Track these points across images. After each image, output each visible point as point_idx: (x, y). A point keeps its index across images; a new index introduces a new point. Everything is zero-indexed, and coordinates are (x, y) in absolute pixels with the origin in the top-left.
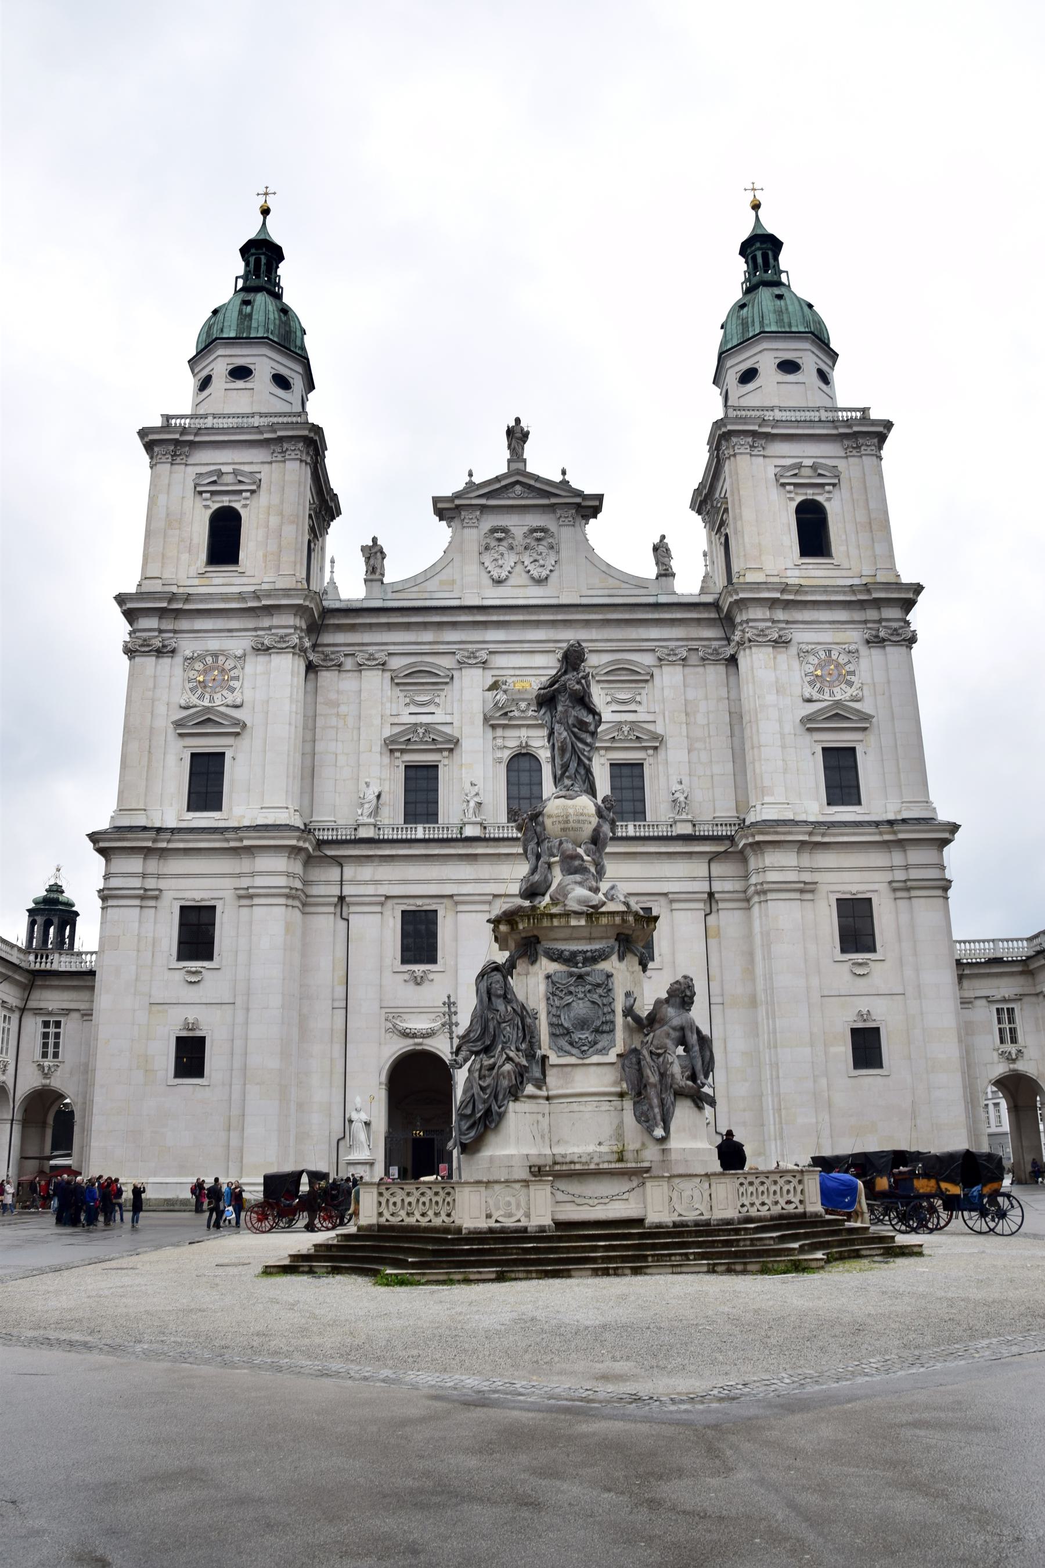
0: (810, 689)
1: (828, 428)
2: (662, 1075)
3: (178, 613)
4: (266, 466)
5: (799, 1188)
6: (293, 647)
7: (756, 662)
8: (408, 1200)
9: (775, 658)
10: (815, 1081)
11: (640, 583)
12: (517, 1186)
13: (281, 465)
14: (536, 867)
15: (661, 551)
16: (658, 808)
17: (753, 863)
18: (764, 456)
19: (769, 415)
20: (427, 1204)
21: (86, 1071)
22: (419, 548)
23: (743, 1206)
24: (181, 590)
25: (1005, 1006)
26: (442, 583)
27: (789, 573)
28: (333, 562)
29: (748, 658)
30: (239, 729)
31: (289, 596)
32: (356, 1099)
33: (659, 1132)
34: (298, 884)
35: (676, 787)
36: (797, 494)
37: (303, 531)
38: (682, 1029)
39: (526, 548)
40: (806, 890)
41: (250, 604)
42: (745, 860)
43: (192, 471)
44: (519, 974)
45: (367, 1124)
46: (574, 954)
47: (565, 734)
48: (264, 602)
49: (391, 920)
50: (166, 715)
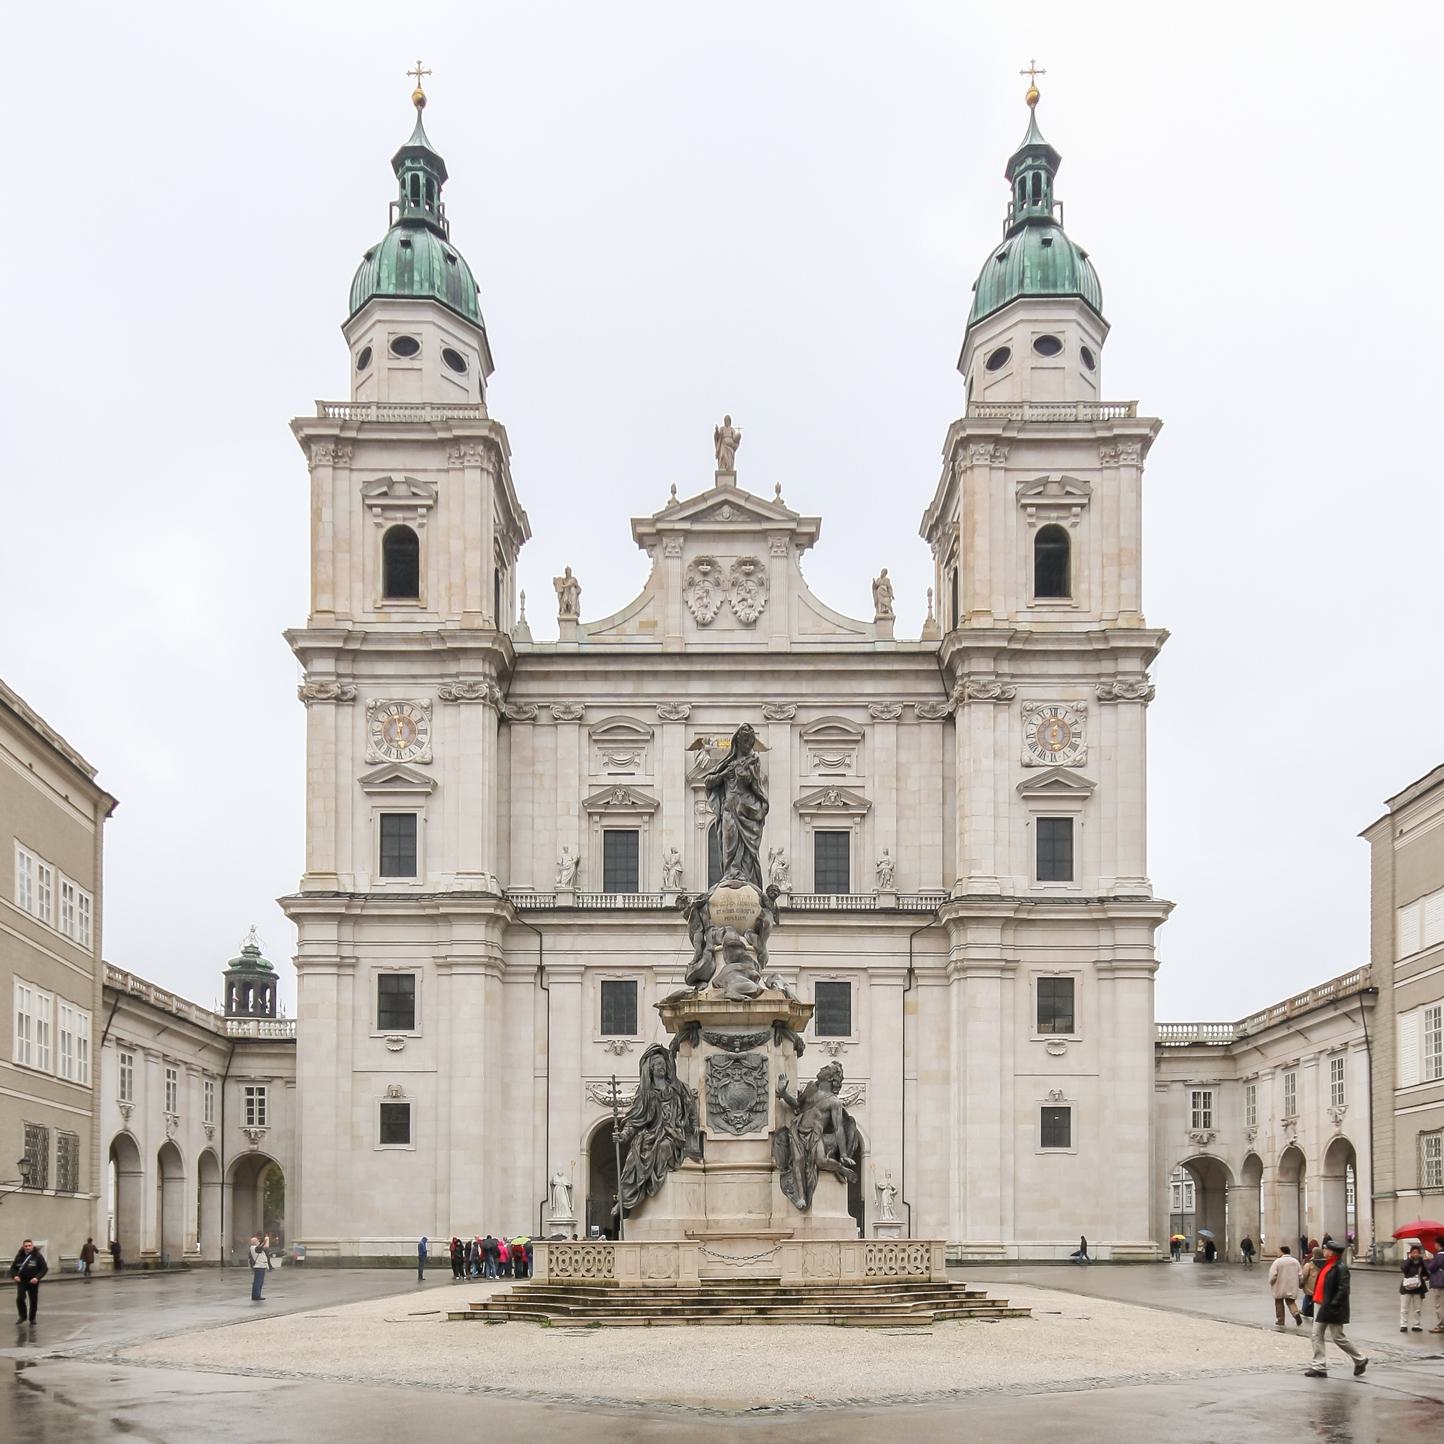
0: (1030, 753)
1: (1084, 431)
2: (807, 1152)
3: (356, 655)
4: (443, 475)
5: (926, 1256)
6: (484, 698)
7: (974, 721)
8: (575, 1258)
9: (995, 717)
10: (1002, 1157)
11: (857, 628)
12: (670, 1247)
13: (460, 473)
14: (702, 955)
15: (882, 589)
16: (863, 881)
17: (955, 940)
18: (1006, 470)
19: (1016, 415)
20: (591, 1261)
21: (293, 1136)
22: (616, 584)
23: (870, 1269)
24: (358, 628)
25: (1202, 1091)
26: (642, 624)
27: (1020, 617)
28: (523, 597)
29: (966, 717)
30: (430, 789)
31: (476, 638)
32: (557, 1163)
33: (802, 1202)
34: (497, 954)
35: (882, 858)
36: (1038, 518)
37: (488, 557)
38: (829, 1110)
39: (733, 584)
40: (1008, 968)
41: (434, 647)
42: (948, 936)
43: (359, 478)
44: (681, 1056)
45: (569, 1188)
46: (732, 1039)
47: (732, 822)
48: (449, 645)
49: (591, 990)
50: (350, 774)
